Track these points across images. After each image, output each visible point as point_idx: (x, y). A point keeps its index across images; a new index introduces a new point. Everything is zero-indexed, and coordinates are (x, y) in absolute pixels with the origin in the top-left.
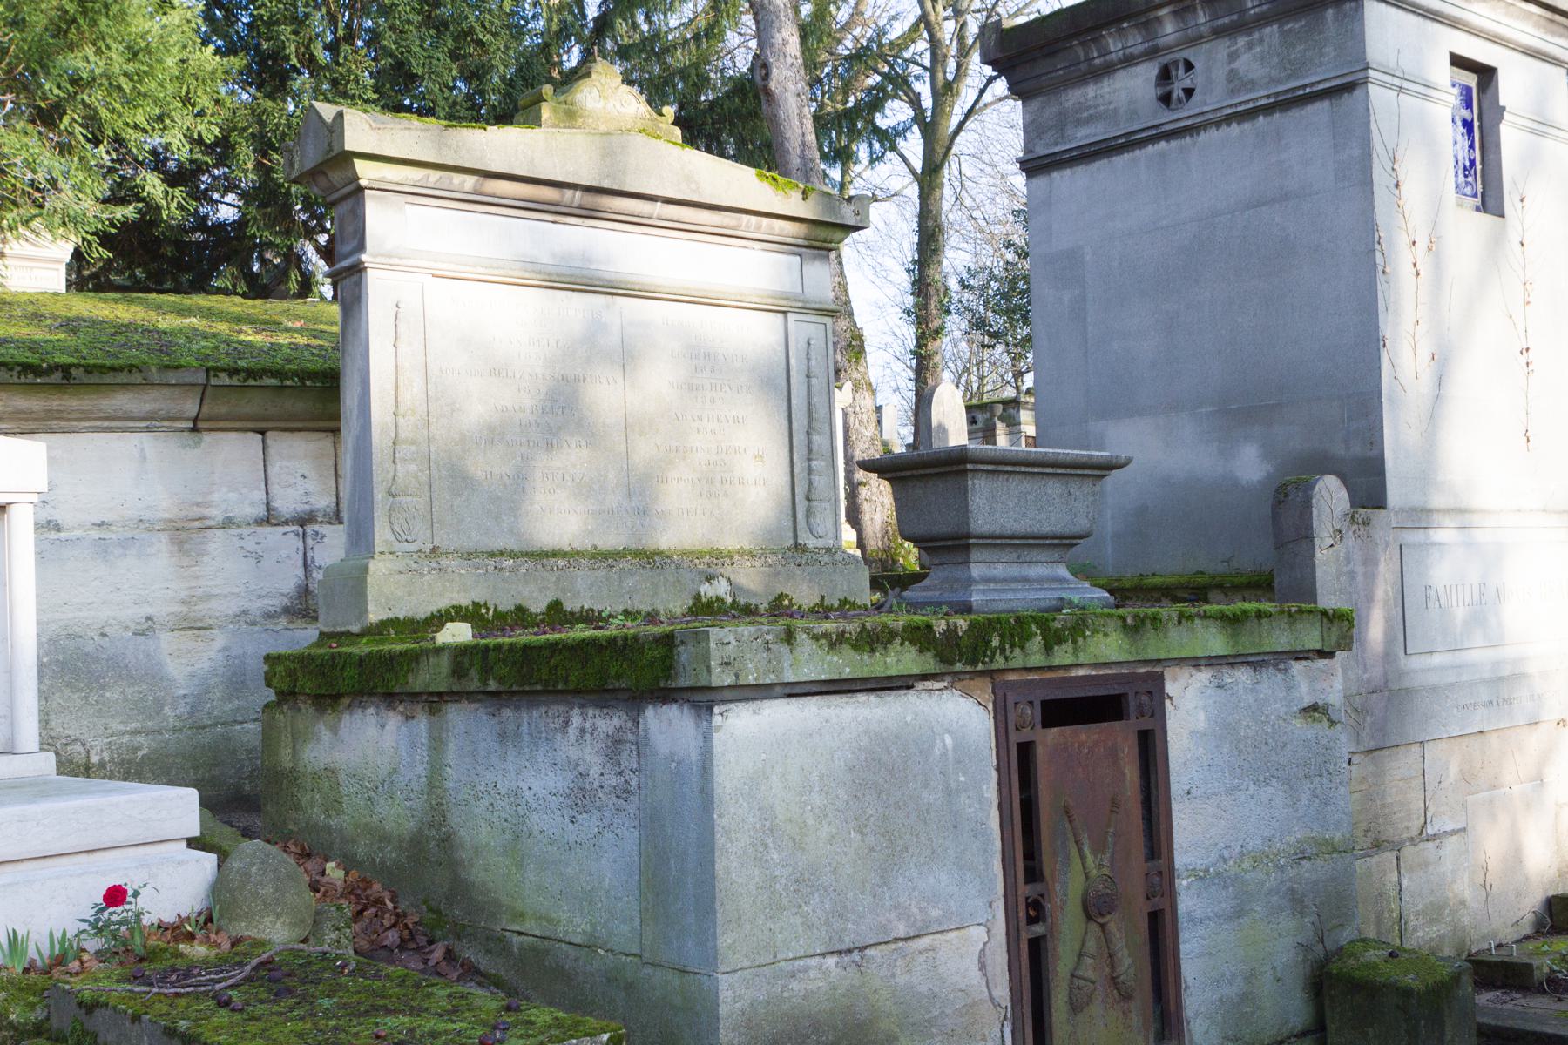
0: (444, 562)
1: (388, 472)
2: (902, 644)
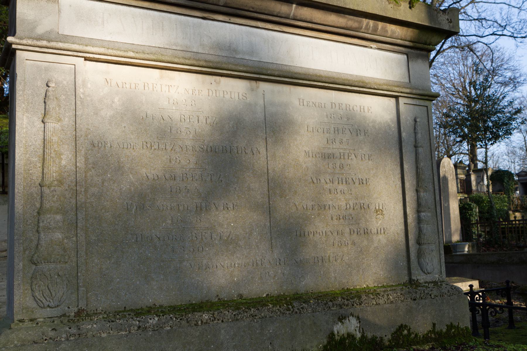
0: (87, 326)
1: (31, 241)
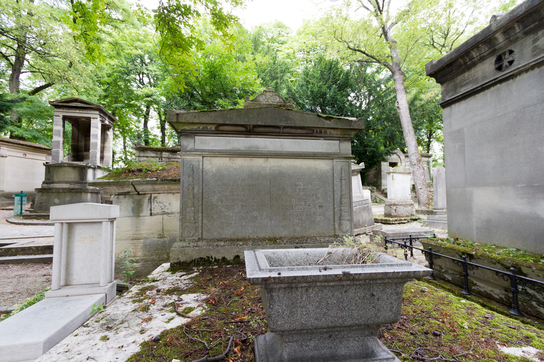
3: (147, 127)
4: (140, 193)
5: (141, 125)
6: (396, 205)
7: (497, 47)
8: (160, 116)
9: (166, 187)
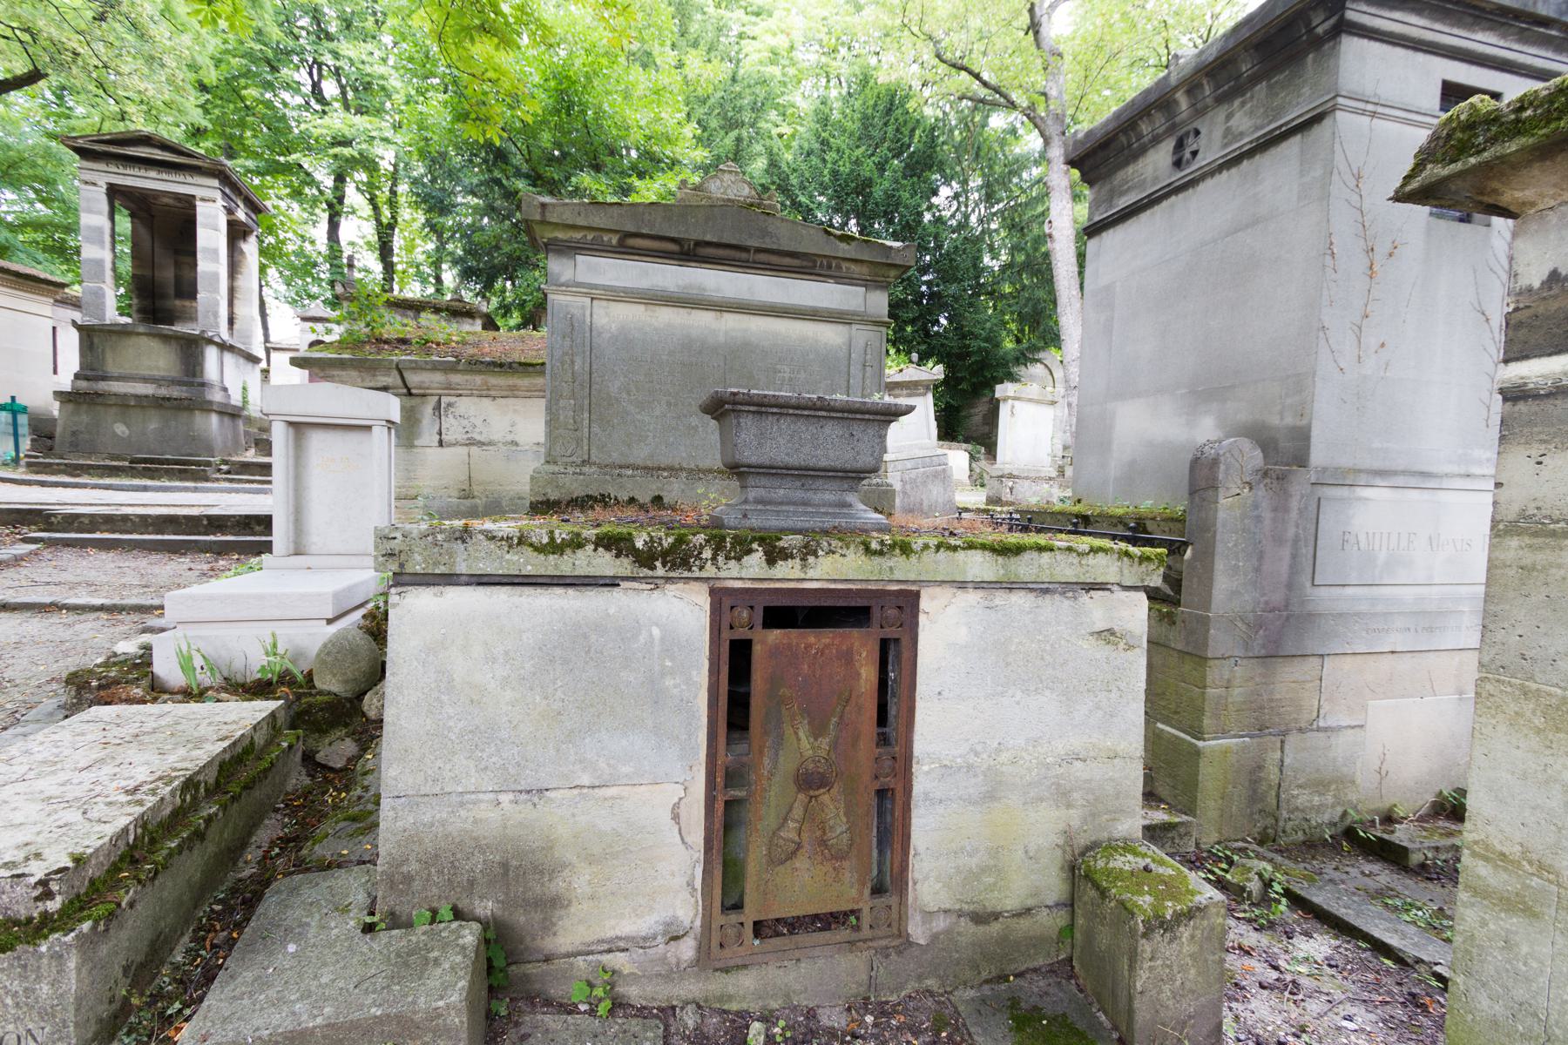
2: (595, 550)
3: (338, 242)
4: (413, 391)
5: (320, 232)
6: (1015, 477)
7: (1178, 119)
8: (376, 208)
9: (478, 379)
